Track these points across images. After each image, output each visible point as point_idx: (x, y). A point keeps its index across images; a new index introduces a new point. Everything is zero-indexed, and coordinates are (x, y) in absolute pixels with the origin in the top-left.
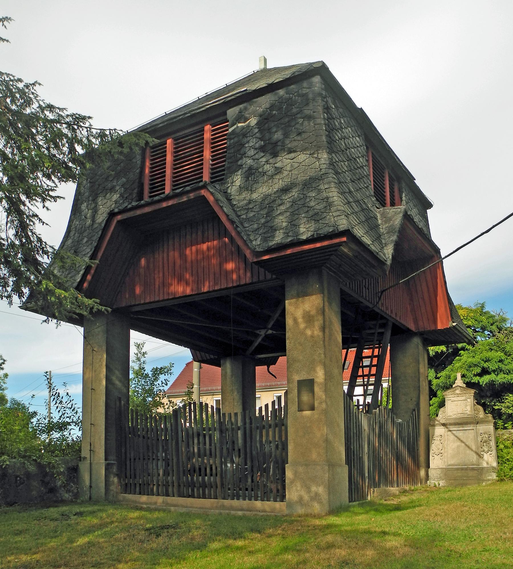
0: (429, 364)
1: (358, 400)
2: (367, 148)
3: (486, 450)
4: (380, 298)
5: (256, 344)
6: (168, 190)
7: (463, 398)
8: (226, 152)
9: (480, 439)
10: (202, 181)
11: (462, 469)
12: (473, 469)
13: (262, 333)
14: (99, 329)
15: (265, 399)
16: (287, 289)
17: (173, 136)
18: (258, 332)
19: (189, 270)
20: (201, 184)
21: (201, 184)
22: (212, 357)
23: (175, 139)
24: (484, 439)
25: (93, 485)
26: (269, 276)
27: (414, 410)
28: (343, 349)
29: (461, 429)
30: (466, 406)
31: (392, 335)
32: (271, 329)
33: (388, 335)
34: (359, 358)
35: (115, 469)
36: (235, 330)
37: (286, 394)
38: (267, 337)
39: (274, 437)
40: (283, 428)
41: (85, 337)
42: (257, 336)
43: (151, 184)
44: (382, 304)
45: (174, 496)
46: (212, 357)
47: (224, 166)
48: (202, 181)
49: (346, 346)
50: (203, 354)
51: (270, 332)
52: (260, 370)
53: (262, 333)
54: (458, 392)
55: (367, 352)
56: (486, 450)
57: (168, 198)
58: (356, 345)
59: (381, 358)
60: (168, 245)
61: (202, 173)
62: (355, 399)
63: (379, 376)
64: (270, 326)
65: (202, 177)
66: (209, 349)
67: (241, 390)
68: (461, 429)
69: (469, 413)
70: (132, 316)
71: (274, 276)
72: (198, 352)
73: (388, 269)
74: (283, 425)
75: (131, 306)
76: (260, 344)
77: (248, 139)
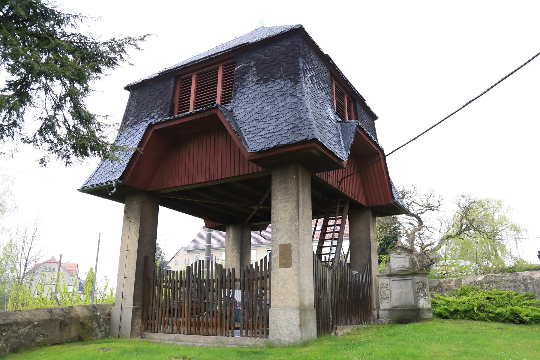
0: (290, 251)
1: (325, 257)
2: (332, 81)
3: (422, 295)
4: (340, 184)
5: (251, 216)
6: (191, 110)
7: (403, 256)
8: (233, 84)
9: (417, 287)
10: (215, 103)
11: (404, 310)
12: (412, 310)
13: (256, 208)
14: (136, 206)
15: (256, 256)
16: (273, 178)
17: (198, 72)
18: (252, 207)
19: (201, 166)
20: (215, 105)
21: (215, 105)
22: (219, 224)
23: (198, 75)
24: (420, 287)
25: (122, 326)
26: (260, 169)
27: (367, 264)
28: (313, 219)
29: (402, 279)
30: (406, 261)
31: (350, 209)
32: (262, 205)
33: (346, 210)
34: (325, 226)
35: (140, 313)
36: (236, 207)
37: (270, 254)
38: (259, 211)
39: (160, 290)
40: (268, 279)
41: (125, 212)
42: (253, 210)
43: (179, 105)
44: (342, 188)
45: (184, 334)
46: (219, 224)
47: (231, 93)
48: (215, 103)
49: (316, 217)
50: (213, 223)
51: (261, 207)
52: (255, 235)
53: (256, 208)
54: (399, 251)
55: (331, 222)
56: (422, 295)
57: (191, 114)
58: (323, 216)
59: (342, 225)
60: (186, 152)
61: (216, 97)
62: (323, 256)
63: (340, 240)
64: (261, 203)
65: (216, 100)
66: (215, 220)
67: (239, 249)
68: (402, 279)
69: (408, 267)
70: (161, 196)
71: (264, 169)
72: (209, 221)
73: (345, 164)
74: (268, 278)
75: (160, 190)
76: (254, 216)
77: (249, 75)
